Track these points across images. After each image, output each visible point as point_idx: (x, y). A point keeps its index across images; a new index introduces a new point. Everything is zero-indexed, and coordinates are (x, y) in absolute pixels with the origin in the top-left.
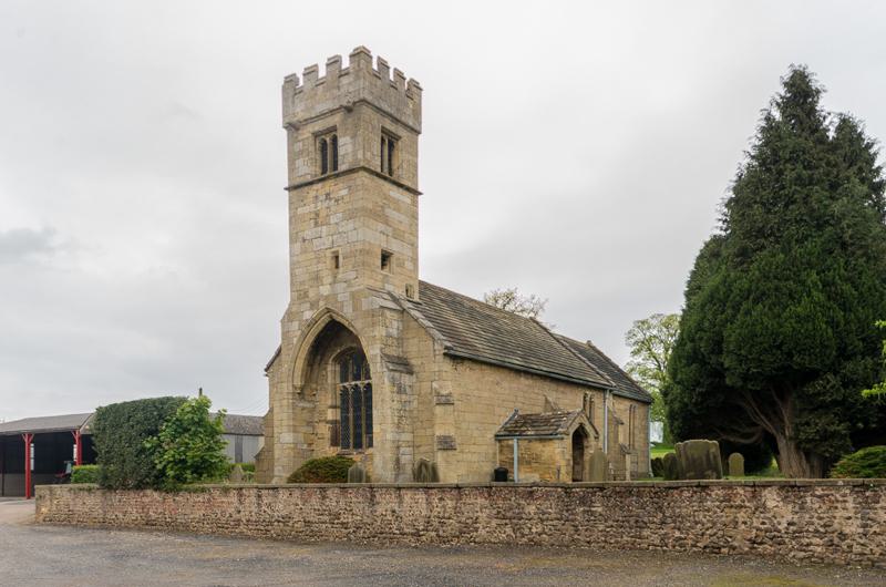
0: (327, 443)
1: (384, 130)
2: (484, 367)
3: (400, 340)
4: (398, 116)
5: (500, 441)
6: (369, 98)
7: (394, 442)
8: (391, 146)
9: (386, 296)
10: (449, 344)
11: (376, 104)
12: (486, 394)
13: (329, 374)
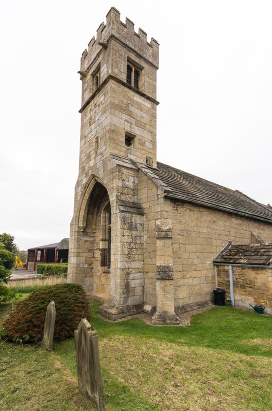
0: (99, 263)
1: (129, 60)
2: (201, 209)
3: (135, 191)
4: (141, 53)
5: (218, 266)
6: (117, 36)
7: (123, 269)
8: (137, 75)
9: (129, 162)
10: (168, 189)
11: (123, 40)
12: (205, 230)
13: (102, 219)
